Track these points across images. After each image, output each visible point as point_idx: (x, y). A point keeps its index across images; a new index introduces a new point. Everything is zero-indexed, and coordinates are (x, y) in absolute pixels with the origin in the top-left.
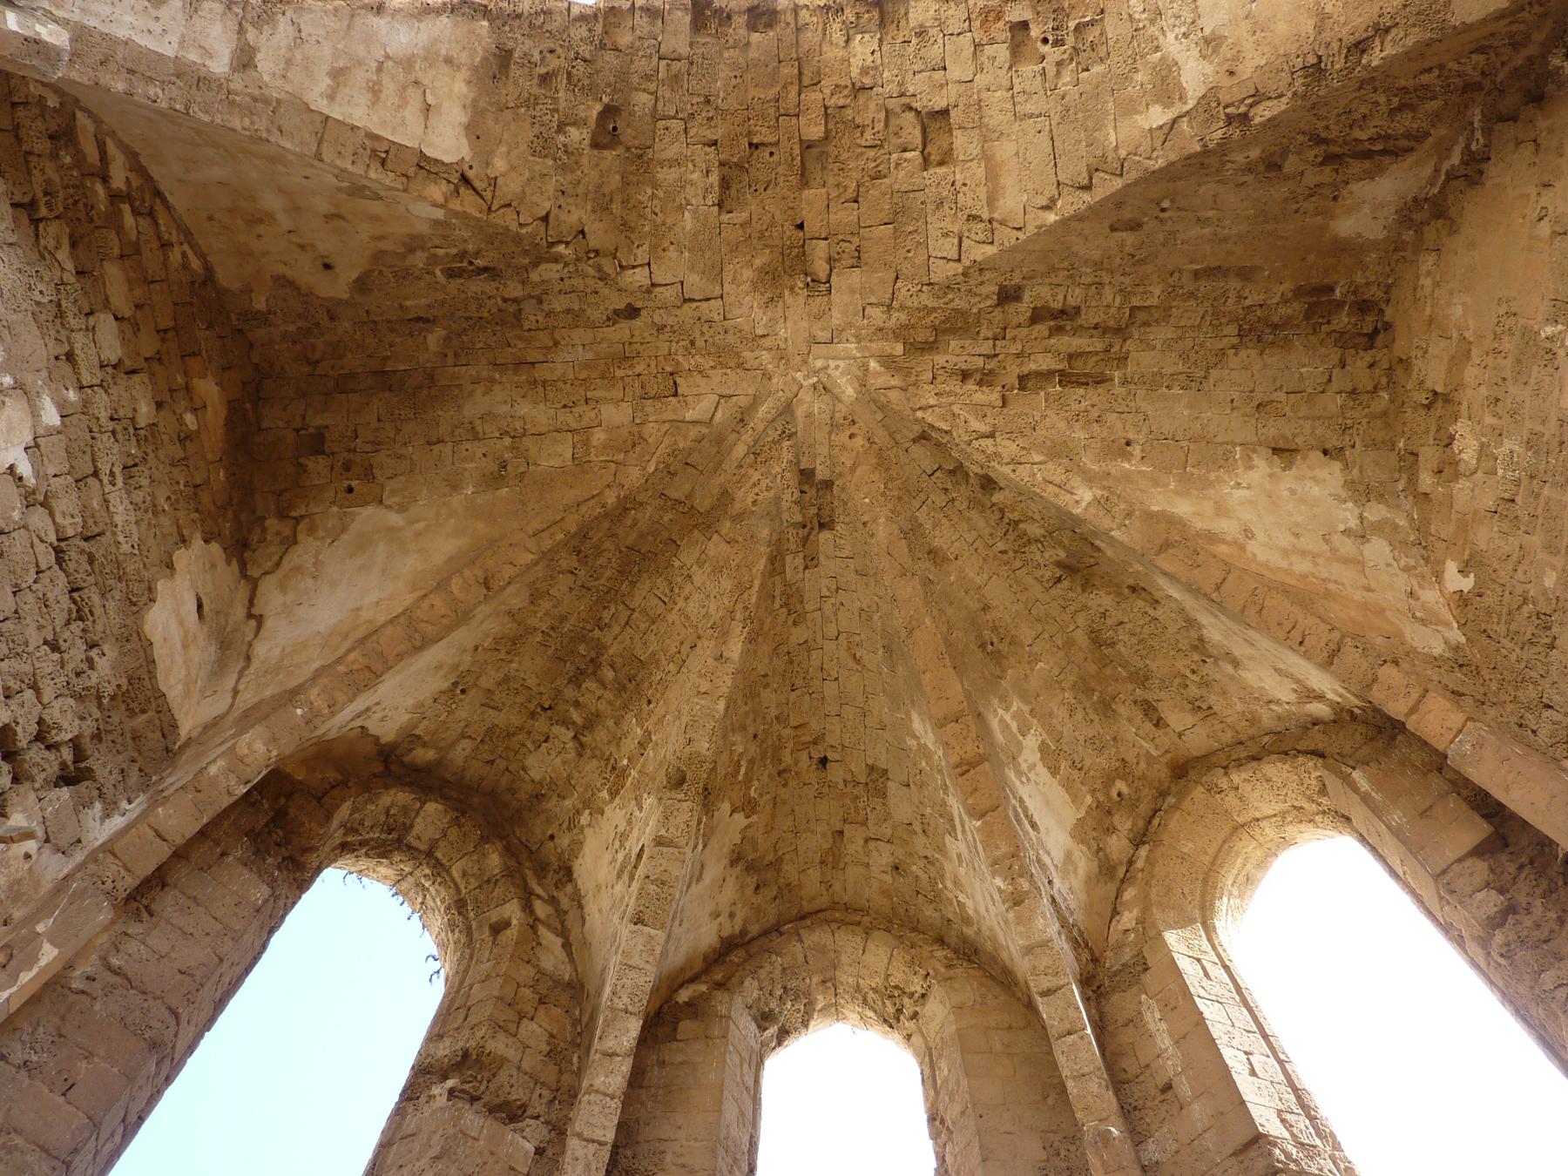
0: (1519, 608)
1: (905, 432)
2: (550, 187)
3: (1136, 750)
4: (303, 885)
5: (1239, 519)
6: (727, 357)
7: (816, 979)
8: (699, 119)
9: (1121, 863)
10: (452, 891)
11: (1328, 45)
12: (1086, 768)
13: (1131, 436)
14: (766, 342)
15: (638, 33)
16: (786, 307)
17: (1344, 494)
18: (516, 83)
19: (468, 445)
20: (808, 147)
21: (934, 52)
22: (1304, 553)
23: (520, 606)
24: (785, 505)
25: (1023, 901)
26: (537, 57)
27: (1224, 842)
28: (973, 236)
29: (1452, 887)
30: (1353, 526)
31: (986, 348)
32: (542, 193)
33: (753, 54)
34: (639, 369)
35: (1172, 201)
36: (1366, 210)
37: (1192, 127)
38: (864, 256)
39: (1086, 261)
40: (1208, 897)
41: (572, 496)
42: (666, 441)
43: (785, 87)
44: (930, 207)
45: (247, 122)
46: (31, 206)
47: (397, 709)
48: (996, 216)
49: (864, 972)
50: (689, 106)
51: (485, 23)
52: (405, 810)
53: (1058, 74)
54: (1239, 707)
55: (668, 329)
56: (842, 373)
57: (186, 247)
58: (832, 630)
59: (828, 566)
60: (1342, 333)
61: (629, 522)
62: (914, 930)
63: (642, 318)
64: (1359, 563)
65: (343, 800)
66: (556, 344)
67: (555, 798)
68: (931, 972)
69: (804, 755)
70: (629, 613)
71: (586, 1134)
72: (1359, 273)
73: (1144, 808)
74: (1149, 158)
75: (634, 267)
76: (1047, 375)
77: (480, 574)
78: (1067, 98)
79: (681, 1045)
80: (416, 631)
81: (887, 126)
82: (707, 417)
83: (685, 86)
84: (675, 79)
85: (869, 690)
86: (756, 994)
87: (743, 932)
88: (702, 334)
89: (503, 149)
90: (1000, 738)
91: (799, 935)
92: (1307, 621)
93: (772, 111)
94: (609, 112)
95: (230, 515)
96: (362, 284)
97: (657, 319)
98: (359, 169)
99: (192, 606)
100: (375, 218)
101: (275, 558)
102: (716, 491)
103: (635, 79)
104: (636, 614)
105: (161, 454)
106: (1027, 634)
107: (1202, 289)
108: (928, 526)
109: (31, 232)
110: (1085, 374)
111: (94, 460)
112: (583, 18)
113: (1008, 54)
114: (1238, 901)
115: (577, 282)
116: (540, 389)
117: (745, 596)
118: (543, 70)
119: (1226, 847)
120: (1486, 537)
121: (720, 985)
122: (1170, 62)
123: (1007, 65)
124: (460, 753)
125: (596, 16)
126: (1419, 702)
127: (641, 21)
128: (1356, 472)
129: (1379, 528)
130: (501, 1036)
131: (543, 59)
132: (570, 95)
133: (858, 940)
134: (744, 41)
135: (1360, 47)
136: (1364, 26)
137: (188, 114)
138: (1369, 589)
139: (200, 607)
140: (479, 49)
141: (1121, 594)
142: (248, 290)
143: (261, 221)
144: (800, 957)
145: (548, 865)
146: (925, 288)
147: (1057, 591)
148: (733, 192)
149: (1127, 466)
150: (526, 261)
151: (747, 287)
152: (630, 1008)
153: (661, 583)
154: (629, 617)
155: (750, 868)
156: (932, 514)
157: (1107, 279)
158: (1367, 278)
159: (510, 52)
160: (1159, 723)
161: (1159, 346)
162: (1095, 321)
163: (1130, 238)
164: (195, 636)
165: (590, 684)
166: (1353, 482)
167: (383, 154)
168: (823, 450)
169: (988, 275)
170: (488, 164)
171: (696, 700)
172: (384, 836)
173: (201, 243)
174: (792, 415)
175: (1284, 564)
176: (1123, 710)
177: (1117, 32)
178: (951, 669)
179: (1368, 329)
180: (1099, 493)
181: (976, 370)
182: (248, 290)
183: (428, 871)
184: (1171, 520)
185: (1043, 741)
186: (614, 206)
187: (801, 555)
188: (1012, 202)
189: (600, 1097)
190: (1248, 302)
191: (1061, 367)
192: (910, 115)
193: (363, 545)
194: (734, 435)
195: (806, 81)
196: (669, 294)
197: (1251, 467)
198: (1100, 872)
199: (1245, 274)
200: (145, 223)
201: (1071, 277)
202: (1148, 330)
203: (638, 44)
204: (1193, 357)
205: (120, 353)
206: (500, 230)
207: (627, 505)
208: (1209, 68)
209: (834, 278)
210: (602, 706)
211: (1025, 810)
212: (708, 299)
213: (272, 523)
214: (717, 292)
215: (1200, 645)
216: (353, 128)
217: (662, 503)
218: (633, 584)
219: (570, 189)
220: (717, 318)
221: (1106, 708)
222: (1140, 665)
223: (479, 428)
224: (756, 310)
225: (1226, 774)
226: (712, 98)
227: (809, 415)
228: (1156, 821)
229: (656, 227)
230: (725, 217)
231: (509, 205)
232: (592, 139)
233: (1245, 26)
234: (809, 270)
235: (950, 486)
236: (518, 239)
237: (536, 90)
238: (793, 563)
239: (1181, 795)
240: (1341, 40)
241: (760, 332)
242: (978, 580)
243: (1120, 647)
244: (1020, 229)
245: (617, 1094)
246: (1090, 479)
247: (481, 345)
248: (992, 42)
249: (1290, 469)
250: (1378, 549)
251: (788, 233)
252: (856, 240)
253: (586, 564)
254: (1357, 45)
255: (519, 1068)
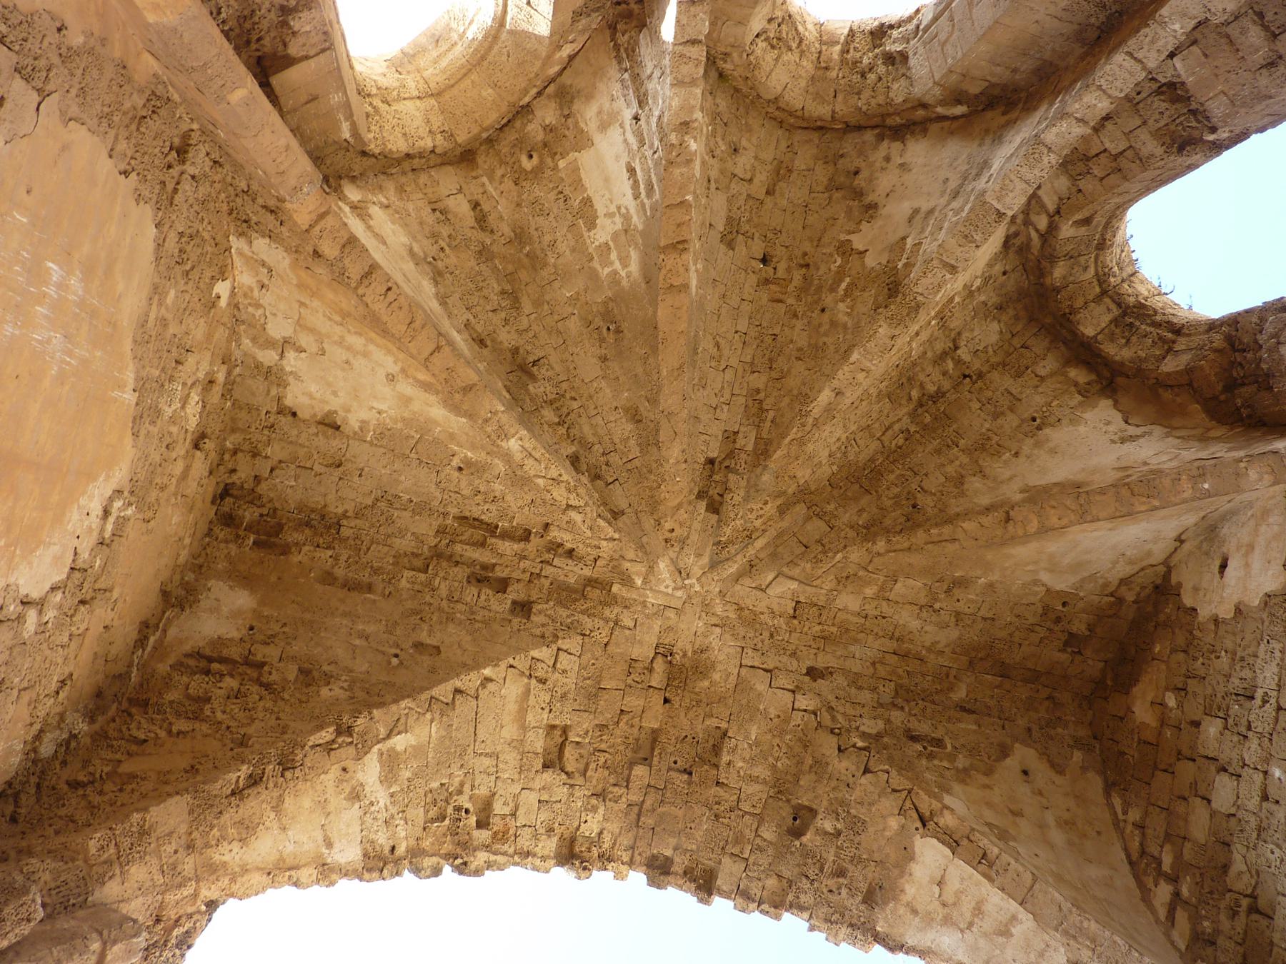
0: (193, 268)
1: (628, 522)
2: (857, 794)
3: (502, 187)
4: (1234, 321)
5: (393, 390)
6: (748, 618)
7: (833, 74)
8: (727, 806)
9: (549, 97)
10: (1101, 258)
11: (275, 786)
12: (555, 192)
13: (456, 474)
14: (714, 620)
15: (760, 884)
16: (693, 643)
17: (291, 379)
18: (865, 878)
19: (967, 611)
20: (646, 759)
21: (544, 815)
22: (349, 348)
23: (974, 479)
24: (742, 493)
25: (681, 124)
26: (844, 891)
27: (452, 86)
28: (545, 667)
29: (323, 37)
30: (292, 352)
31: (548, 570)
32: (865, 790)
33: (673, 841)
34: (818, 628)
35: (390, 663)
36: (225, 610)
37: (377, 729)
38: (626, 667)
39: (460, 623)
40: (486, 45)
41: (915, 559)
42: (820, 572)
43: (654, 810)
44: (571, 696)
45: (1086, 924)
46: (1253, 909)
47: (1095, 427)
48: (526, 680)
49: (793, 67)
50: (732, 818)
51: (878, 929)
52: (1112, 338)
53: (462, 784)
54: (410, 206)
55: (788, 653)
56: (664, 581)
57: (1121, 817)
58: (729, 375)
59: (716, 429)
60: (251, 502)
61: (865, 515)
62: (737, 90)
63: (805, 666)
64: (300, 324)
65: (1169, 374)
66: (873, 664)
67: (989, 304)
68: (745, 56)
69: (780, 273)
70: (883, 438)
71: (1139, 67)
72: (233, 554)
73: (511, 136)
74: (410, 708)
75: (805, 711)
76: (506, 535)
77: (1010, 526)
78: (459, 765)
79: (989, 78)
80: (1081, 505)
81: (587, 765)
82: (780, 579)
83: (731, 833)
84: (738, 840)
85: (715, 317)
86: (895, 86)
87: (881, 138)
88: (763, 641)
89: (887, 834)
90: (634, 255)
91: (832, 117)
92: (379, 307)
93: (668, 795)
94: (797, 833)
95: (1162, 617)
96: (1004, 752)
97: (795, 663)
98: (1005, 858)
99: (1229, 571)
100: (989, 805)
101: (1142, 574)
102: (788, 517)
103: (770, 851)
104: (878, 435)
105: (1209, 691)
106: (574, 325)
107: (367, 575)
108: (632, 442)
109: (1258, 891)
110: (475, 528)
111: (1277, 720)
112: (801, 908)
113: (495, 806)
114: (454, 25)
115: (851, 711)
116: (897, 634)
117: (800, 435)
118: (841, 880)
119: (452, 82)
120: (198, 329)
121: (924, 106)
122: (385, 784)
123: (496, 797)
124: (1048, 365)
125: (791, 906)
126: (316, 222)
127: (755, 891)
128: (274, 392)
129: (270, 344)
130: (1145, 152)
131: (839, 888)
132: (825, 855)
133: (786, 97)
134: (678, 852)
135: (255, 781)
136: (250, 798)
137: (1130, 946)
138: (302, 304)
139: (1223, 566)
140: (888, 912)
141: (493, 341)
142: (1084, 769)
143: (1066, 823)
144: (840, 98)
145: (1017, 252)
146: (588, 633)
147: (539, 353)
148: (711, 742)
149: (469, 454)
150: (886, 740)
151: (719, 667)
152: (1046, 151)
153: (851, 457)
154: (883, 434)
155: (858, 194)
156: (626, 450)
157: (445, 604)
158: (227, 548)
159: (864, 901)
160: (475, 206)
161: (409, 534)
162: (456, 570)
163: (424, 637)
164: (1238, 549)
165: (931, 389)
166: (279, 385)
167: (983, 861)
168: (697, 525)
169: (538, 632)
170: (903, 827)
171: (873, 368)
172: (1137, 323)
173: (1108, 815)
174: (711, 559)
175: (371, 347)
176: (506, 229)
177: (416, 812)
178: (660, 326)
179: (229, 500)
180: (504, 444)
181: (560, 556)
182: (1084, 769)
183: (1112, 279)
184: (456, 409)
185: (589, 230)
186: (810, 762)
187: (737, 446)
188: (513, 689)
189: (1110, 92)
190: (330, 553)
191: (493, 540)
192: (569, 768)
193: (1077, 566)
194: (762, 555)
195: (636, 809)
196: (783, 681)
197: (363, 422)
198: (573, 97)
199: (328, 578)
200: (1153, 849)
201: (473, 613)
202: (415, 551)
203: (762, 876)
204: (383, 519)
205: (1218, 778)
206: (903, 772)
207: (869, 531)
208: (360, 776)
209: (652, 655)
210: (929, 369)
211: (636, 185)
212: (751, 667)
213: (1130, 597)
214: (744, 671)
215: (437, 276)
216: (1003, 890)
217: (833, 521)
218: (872, 460)
219: (843, 787)
220: (750, 651)
221: (520, 236)
222: (483, 267)
223: (953, 619)
224: (717, 648)
225: (434, 147)
226: (713, 818)
227: (699, 555)
228: (505, 120)
229: (781, 736)
230: (724, 725)
231: (894, 791)
232: (815, 817)
233: (331, 807)
234: (668, 665)
235: (604, 467)
236: (891, 760)
237: (850, 867)
238: (747, 441)
239: (476, 138)
240: (266, 788)
241: (718, 630)
242: (603, 384)
243: (497, 288)
244: (511, 666)
245: (1094, 88)
246: (507, 457)
247: (928, 678)
248: (504, 817)
249: (329, 412)
250: (278, 329)
251: (677, 699)
252: (629, 681)
253: (909, 493)
254: (255, 783)
255: (1145, 123)
